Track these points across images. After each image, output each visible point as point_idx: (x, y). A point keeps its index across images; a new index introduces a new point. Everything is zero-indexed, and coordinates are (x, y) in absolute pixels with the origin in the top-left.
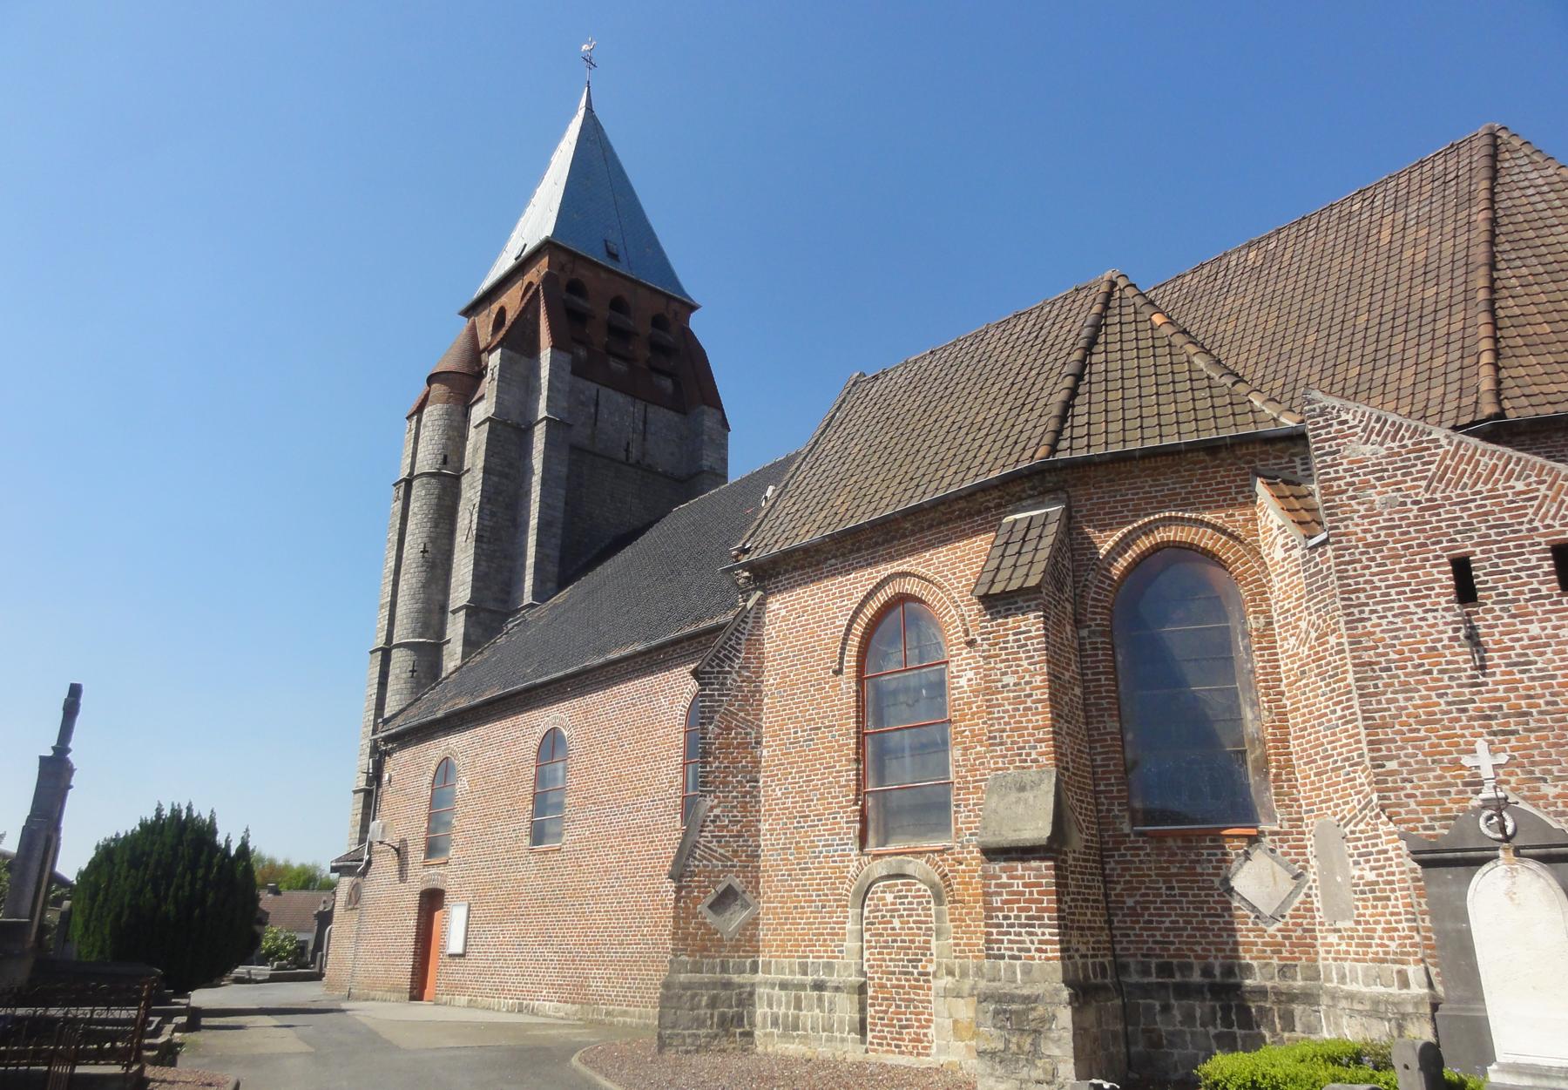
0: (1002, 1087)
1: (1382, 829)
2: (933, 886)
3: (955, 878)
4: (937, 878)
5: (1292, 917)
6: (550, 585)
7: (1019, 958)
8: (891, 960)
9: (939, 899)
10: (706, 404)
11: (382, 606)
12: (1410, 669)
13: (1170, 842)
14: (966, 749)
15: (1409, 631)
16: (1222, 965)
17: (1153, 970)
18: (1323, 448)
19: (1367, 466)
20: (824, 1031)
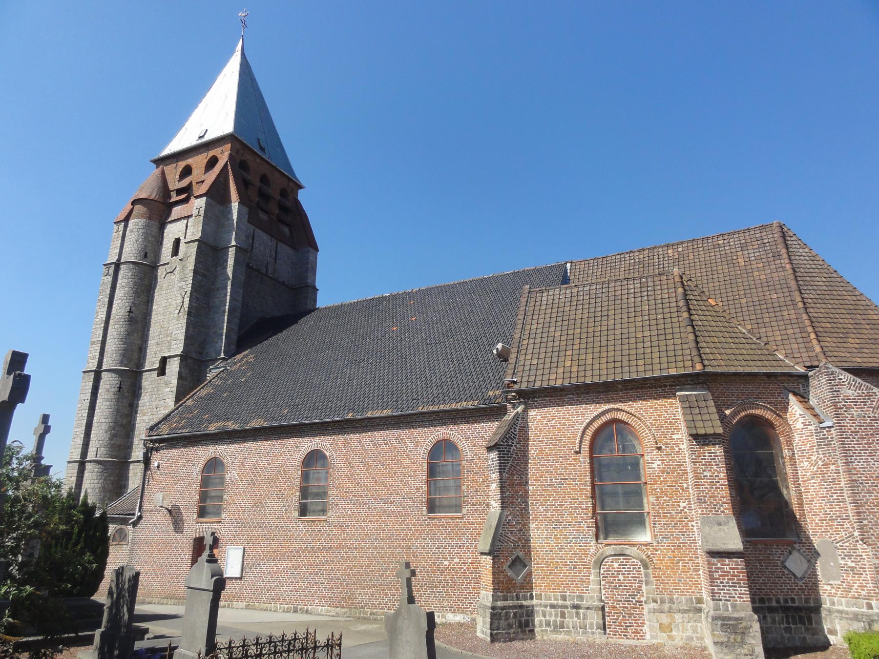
0: (727, 657)
1: (859, 547)
2: (642, 561)
3: (654, 557)
4: (644, 557)
5: (808, 578)
6: (233, 347)
7: (730, 601)
8: (619, 595)
9: (646, 567)
10: (311, 247)
11: (94, 343)
12: (870, 484)
13: (759, 546)
14: (658, 498)
15: (869, 469)
16: (783, 598)
17: (757, 601)
18: (833, 389)
19: (850, 399)
20: (580, 628)
